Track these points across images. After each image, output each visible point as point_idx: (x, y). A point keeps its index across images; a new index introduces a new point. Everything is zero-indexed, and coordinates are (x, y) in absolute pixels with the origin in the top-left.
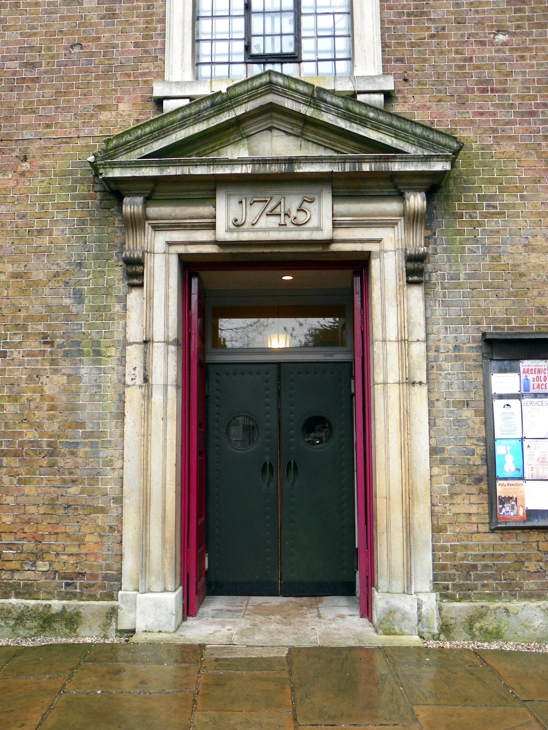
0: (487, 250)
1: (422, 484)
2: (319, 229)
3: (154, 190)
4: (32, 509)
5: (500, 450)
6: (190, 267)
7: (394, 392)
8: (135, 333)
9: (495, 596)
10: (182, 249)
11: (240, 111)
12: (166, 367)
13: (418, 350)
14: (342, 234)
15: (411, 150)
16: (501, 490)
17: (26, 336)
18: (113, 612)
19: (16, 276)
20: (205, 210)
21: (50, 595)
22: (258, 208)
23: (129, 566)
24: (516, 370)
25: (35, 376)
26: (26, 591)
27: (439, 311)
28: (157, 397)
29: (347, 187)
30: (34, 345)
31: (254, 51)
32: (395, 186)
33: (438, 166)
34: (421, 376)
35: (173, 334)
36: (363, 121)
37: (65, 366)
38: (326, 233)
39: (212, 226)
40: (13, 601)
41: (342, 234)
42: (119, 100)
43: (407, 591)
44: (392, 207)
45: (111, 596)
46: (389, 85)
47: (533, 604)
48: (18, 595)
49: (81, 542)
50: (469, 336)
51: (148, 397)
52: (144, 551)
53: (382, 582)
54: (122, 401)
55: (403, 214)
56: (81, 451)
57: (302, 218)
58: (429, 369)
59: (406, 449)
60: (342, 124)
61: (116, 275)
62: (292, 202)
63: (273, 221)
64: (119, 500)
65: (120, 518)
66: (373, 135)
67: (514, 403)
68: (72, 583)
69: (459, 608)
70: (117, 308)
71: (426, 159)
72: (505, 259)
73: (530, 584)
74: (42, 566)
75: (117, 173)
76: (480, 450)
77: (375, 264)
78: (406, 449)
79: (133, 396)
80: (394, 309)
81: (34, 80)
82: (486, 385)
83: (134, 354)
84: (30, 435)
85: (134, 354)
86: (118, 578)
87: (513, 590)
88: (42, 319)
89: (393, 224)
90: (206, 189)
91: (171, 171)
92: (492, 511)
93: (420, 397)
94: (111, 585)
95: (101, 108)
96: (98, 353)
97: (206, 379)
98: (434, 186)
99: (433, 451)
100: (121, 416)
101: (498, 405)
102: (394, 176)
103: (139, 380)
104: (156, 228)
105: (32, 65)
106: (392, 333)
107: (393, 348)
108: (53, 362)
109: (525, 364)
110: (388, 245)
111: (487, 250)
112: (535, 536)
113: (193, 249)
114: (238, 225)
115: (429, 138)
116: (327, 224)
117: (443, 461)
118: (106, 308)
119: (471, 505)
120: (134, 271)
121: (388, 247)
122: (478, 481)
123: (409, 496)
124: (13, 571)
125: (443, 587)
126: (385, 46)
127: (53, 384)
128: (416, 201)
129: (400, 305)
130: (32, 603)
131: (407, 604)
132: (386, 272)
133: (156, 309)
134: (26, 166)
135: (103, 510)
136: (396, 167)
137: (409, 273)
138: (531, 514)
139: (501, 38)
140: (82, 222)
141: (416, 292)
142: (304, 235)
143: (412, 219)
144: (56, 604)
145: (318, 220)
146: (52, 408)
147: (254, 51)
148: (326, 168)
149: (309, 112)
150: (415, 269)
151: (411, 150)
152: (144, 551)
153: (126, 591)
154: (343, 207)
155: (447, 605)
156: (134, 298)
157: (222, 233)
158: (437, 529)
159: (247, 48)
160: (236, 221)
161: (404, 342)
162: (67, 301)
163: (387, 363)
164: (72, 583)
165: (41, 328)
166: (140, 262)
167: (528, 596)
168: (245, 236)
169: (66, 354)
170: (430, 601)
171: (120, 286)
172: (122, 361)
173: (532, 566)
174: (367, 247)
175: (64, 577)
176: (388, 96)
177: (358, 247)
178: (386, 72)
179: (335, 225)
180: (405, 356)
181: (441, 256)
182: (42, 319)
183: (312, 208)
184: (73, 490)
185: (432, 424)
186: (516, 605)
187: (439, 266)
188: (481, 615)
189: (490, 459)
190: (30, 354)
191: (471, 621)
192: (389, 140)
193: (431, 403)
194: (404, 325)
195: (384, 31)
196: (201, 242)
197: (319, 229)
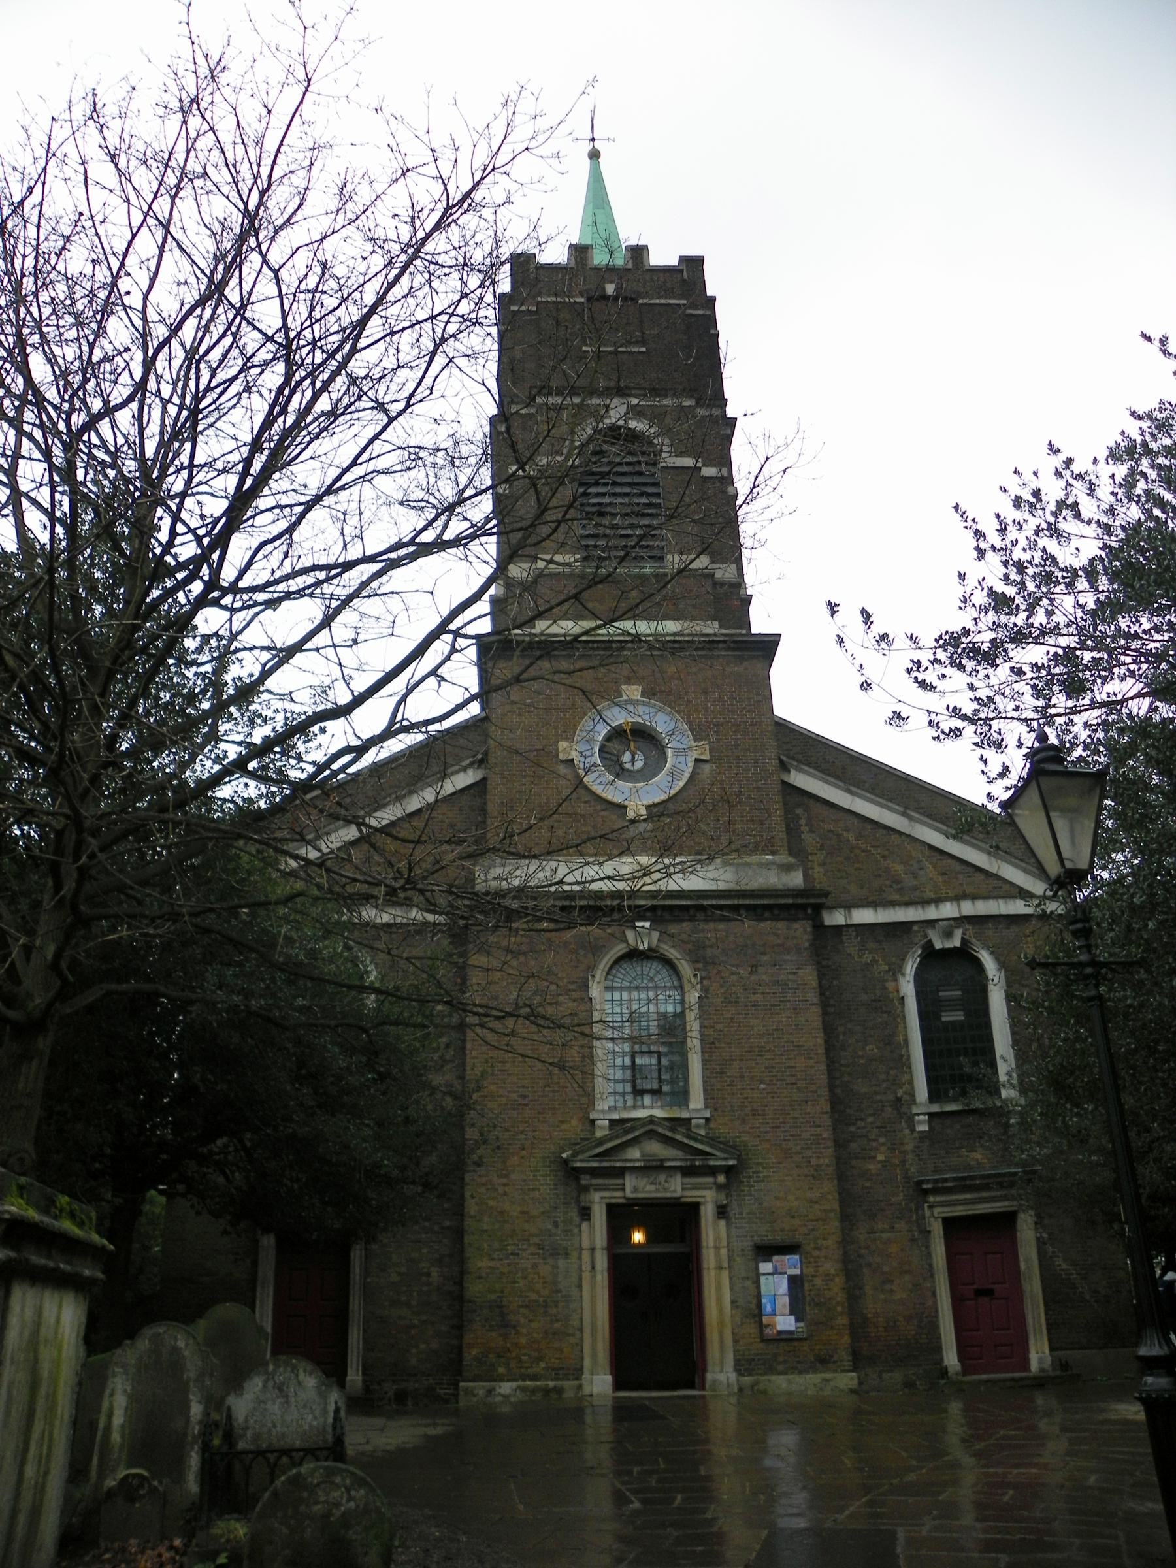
0: (756, 1199)
1: (728, 1320)
2: (675, 1191)
3: (594, 1172)
4: (535, 1335)
5: (764, 1301)
6: (611, 1209)
7: (713, 1273)
8: (586, 1243)
9: (765, 1374)
10: (608, 1201)
11: (637, 1133)
12: (602, 1261)
13: (724, 1251)
14: (687, 1193)
15: (718, 1153)
16: (765, 1320)
17: (529, 1245)
18: (580, 1387)
19: (522, 1212)
20: (619, 1181)
21: (547, 1380)
22: (645, 1180)
23: (587, 1363)
24: (770, 1261)
25: (535, 1266)
26: (534, 1378)
27: (733, 1230)
28: (599, 1277)
29: (688, 1171)
30: (532, 1249)
31: (638, 1088)
32: (713, 1171)
33: (731, 1162)
34: (726, 1265)
35: (605, 1244)
36: (696, 1140)
37: (550, 1261)
38: (678, 1194)
39: (623, 1190)
40: (528, 1383)
41: (687, 1193)
42: (572, 1118)
43: (722, 1371)
44: (710, 1180)
45: (577, 1379)
46: (708, 1115)
47: (782, 1377)
48: (530, 1380)
49: (562, 1352)
50: (747, 1244)
51: (594, 1277)
52: (594, 1355)
53: (710, 1368)
54: (581, 1279)
55: (715, 1183)
56: (561, 1304)
57: (666, 1185)
58: (729, 1261)
59: (719, 1301)
60: (686, 1141)
61: (574, 1215)
62: (662, 1177)
63: (652, 1188)
64: (581, 1330)
65: (582, 1339)
66: (700, 1146)
67: (770, 1277)
68: (558, 1372)
69: (747, 1380)
70: (576, 1231)
71: (726, 1159)
72: (765, 1204)
73: (781, 1368)
74: (542, 1365)
75: (578, 1164)
76: (755, 1301)
77: (702, 1208)
78: (719, 1301)
79: (586, 1275)
80: (713, 1233)
81: (526, 1105)
82: (757, 1268)
83: (586, 1255)
84: (533, 1296)
85: (586, 1255)
86: (581, 1369)
87: (771, 1370)
88: (537, 1236)
89: (710, 1189)
90: (621, 1172)
91: (605, 1164)
92: (761, 1332)
93: (725, 1275)
94: (577, 1373)
95: (562, 1122)
96: (567, 1254)
97: (623, 1263)
98: (728, 1170)
99: (732, 1302)
100: (580, 1286)
101: (763, 1279)
102: (710, 1167)
103: (589, 1268)
104: (595, 1190)
105: (524, 1097)
106: (711, 1244)
107: (712, 1252)
108: (544, 1259)
109: (775, 1258)
110: (709, 1199)
111: (756, 1199)
112: (782, 1344)
113: (614, 1201)
114: (635, 1190)
115: (729, 1147)
116: (679, 1189)
117: (737, 1307)
118: (570, 1231)
119: (751, 1329)
120: (585, 1213)
121: (708, 1198)
122: (755, 1316)
123: (721, 1324)
124: (527, 1368)
125: (741, 1367)
126: (705, 1090)
127: (545, 1270)
128: (721, 1179)
129: (714, 1229)
130: (538, 1383)
131: (722, 1377)
132: (708, 1212)
133: (597, 1230)
134: (524, 1152)
135: (573, 1335)
136: (712, 1163)
137: (719, 1213)
138: (780, 1332)
139: (762, 1086)
140: (555, 1185)
141: (722, 1223)
142: (668, 1195)
143: (720, 1188)
144: (551, 1384)
145: (675, 1187)
146: (545, 1282)
147: (638, 1088)
148: (678, 1164)
149: (669, 1134)
150: (722, 1212)
151: (718, 1153)
152: (594, 1355)
153: (586, 1375)
154: (687, 1180)
155: (741, 1378)
156: (585, 1226)
157: (629, 1193)
158: (736, 1341)
159: (634, 1086)
160: (635, 1187)
161: (717, 1248)
162: (550, 1227)
163: (709, 1259)
164: (558, 1372)
165: (536, 1240)
166: (589, 1209)
167: (780, 1373)
168: (640, 1195)
169: (551, 1255)
170: (733, 1376)
171: (577, 1219)
172: (580, 1258)
173: (781, 1359)
174: (698, 1200)
175: (554, 1369)
176: (707, 1119)
177: (694, 1200)
178: (706, 1107)
179: (683, 1189)
180: (717, 1255)
181: (735, 1205)
182: (537, 1236)
183: (672, 1180)
184: (557, 1325)
185: (731, 1289)
186: (774, 1378)
187: (734, 1209)
188: (757, 1383)
189: (759, 1305)
190: (532, 1254)
191: (752, 1386)
192: (708, 1149)
193: (731, 1278)
194: (717, 1239)
195: (704, 1082)
196: (617, 1197)
197: (675, 1191)
